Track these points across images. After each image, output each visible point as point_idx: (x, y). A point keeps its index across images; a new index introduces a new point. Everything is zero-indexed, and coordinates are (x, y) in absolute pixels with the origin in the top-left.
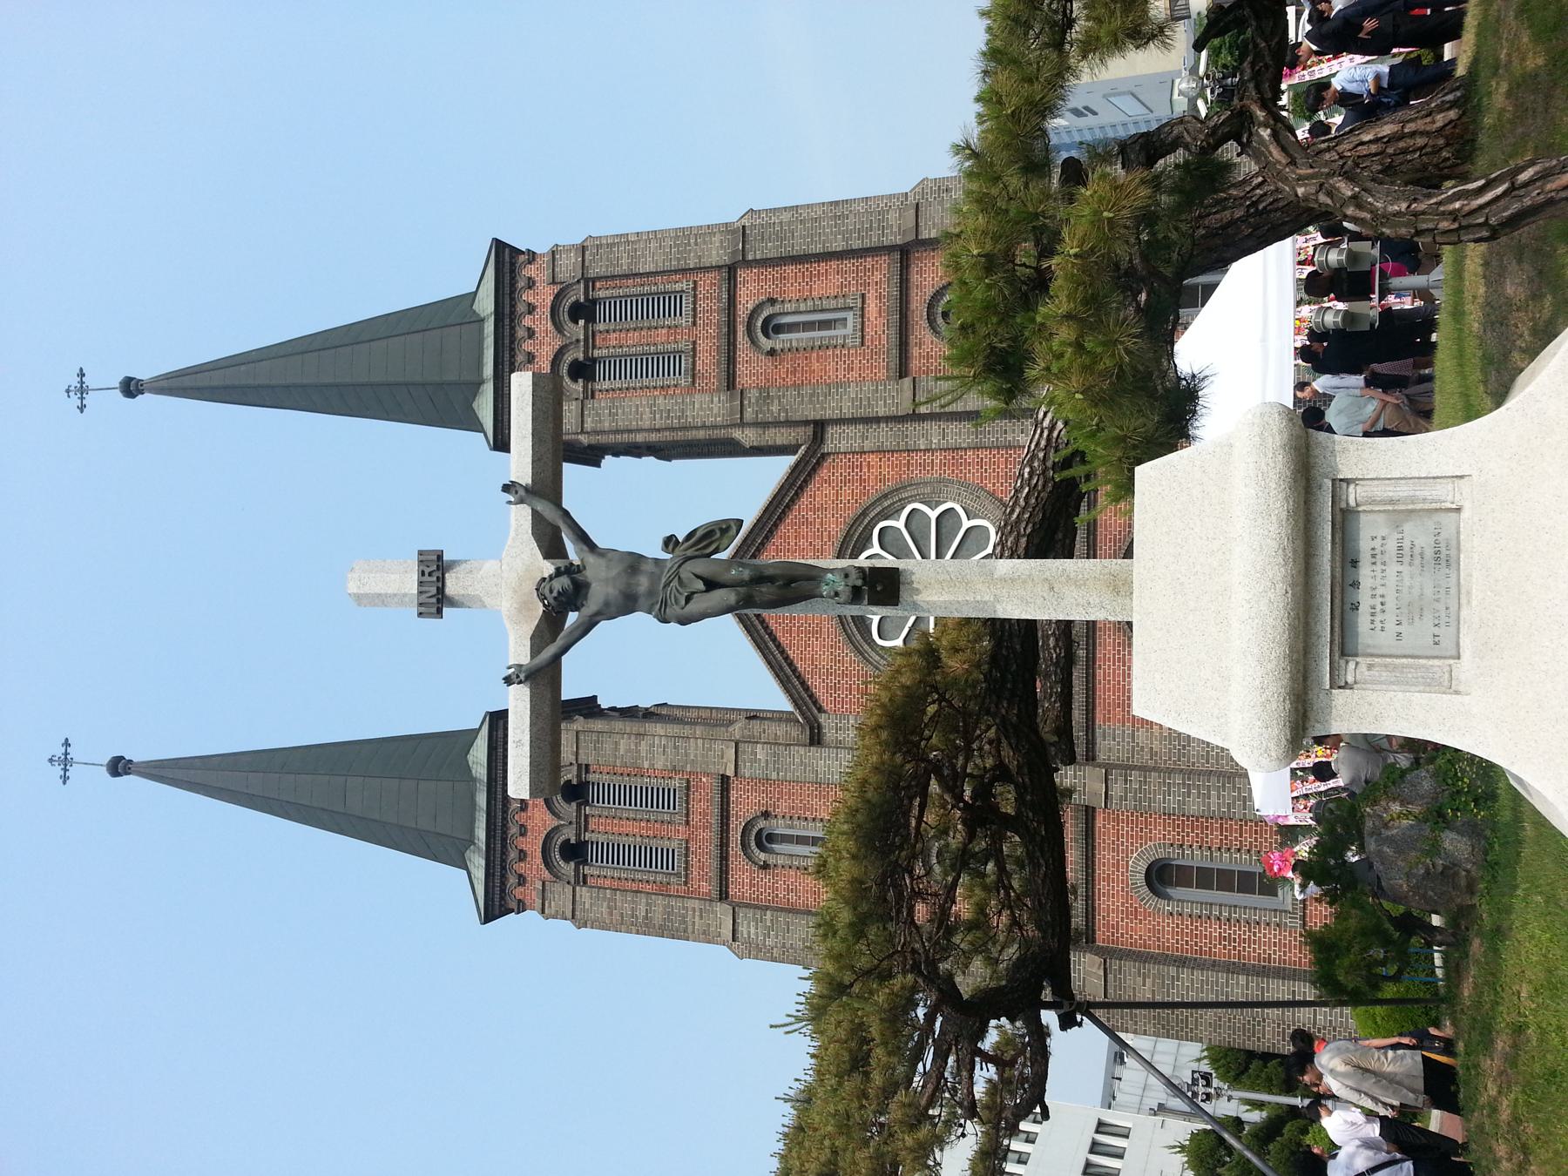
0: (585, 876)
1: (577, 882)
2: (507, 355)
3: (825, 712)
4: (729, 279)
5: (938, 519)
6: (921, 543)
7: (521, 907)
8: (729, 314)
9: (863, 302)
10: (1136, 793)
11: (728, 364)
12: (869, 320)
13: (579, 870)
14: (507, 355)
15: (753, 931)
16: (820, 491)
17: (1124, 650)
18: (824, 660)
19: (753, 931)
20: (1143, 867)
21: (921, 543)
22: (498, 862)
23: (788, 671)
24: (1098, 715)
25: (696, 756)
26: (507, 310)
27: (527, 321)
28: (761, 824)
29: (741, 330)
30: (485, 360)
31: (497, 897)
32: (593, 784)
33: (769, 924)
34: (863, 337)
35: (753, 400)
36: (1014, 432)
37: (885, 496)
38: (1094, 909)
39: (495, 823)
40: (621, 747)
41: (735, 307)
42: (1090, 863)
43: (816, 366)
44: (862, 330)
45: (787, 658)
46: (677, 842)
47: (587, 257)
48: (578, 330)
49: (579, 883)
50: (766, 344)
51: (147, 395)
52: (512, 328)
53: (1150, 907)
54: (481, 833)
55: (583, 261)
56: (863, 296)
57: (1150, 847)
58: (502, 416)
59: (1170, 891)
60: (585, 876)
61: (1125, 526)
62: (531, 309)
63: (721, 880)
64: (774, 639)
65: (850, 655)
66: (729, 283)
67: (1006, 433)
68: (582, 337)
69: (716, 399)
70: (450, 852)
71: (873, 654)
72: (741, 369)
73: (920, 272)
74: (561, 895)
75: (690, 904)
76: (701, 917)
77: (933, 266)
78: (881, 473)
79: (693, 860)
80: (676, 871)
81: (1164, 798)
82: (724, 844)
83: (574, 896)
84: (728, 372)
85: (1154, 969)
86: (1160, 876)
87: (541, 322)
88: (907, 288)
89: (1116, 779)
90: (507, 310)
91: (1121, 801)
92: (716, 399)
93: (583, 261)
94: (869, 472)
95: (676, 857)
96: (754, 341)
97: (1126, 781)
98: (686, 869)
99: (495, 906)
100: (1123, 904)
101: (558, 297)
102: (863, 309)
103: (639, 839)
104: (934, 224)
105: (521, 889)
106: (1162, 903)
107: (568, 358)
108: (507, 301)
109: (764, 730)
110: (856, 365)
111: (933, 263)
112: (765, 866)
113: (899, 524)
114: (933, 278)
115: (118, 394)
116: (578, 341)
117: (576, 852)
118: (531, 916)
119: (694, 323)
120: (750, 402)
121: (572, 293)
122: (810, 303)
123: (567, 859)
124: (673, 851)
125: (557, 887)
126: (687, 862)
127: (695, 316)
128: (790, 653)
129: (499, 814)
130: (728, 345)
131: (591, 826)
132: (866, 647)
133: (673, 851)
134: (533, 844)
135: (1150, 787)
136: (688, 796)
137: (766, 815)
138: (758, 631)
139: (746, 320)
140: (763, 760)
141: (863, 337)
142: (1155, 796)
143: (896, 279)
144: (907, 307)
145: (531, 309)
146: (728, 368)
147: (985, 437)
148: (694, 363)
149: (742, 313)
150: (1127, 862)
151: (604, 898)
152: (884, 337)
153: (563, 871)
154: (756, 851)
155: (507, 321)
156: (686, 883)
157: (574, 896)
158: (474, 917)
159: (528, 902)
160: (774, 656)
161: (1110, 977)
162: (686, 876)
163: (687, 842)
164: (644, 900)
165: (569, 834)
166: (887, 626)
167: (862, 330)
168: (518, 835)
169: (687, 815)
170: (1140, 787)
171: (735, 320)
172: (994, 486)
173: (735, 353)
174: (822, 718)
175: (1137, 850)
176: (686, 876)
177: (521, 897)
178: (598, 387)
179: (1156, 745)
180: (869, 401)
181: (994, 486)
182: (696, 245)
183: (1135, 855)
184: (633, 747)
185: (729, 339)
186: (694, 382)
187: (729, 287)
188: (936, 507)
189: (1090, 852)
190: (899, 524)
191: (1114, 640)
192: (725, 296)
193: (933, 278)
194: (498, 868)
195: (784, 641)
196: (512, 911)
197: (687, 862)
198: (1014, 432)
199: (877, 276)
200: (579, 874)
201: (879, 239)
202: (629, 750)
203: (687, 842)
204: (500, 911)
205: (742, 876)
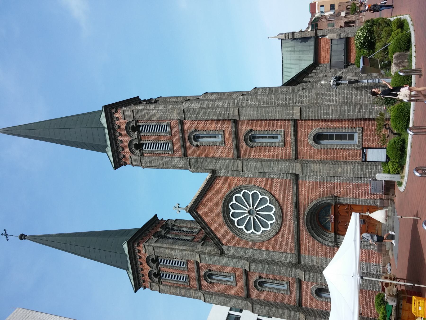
0: (143, 153)
3: (224, 245)
4: (181, 123)
5: (252, 195)
7: (125, 164)
8: (182, 134)
9: (224, 133)
11: (184, 149)
12: (226, 139)
13: (141, 152)
15: (209, 300)
16: (216, 186)
17: (308, 236)
18: (222, 232)
19: (209, 300)
20: (314, 290)
21: (247, 200)
22: (136, 277)
25: (188, 255)
27: (122, 153)
30: (107, 141)
32: (160, 259)
33: (214, 299)
34: (225, 143)
35: (193, 162)
37: (236, 189)
39: (134, 268)
40: (167, 252)
43: (211, 151)
44: (225, 142)
46: (186, 275)
48: (135, 135)
49: (141, 156)
50: (195, 143)
52: (118, 156)
53: (316, 299)
54: (109, 144)
55: (133, 115)
57: (313, 131)
60: (161, 282)
61: (307, 203)
62: (123, 149)
65: (229, 231)
66: (181, 124)
68: (137, 137)
69: (181, 160)
70: (102, 149)
71: (236, 230)
72: (188, 150)
73: (241, 125)
74: (136, 159)
75: (192, 291)
76: (195, 295)
77: (245, 123)
78: (234, 184)
79: (191, 280)
80: (168, 132)
81: (320, 280)
82: (199, 280)
85: (318, 319)
87: (145, 266)
89: (307, 274)
90: (111, 128)
91: (308, 280)
92: (181, 160)
93: (133, 115)
95: (170, 147)
96: (191, 143)
97: (310, 275)
98: (189, 282)
100: (309, 298)
102: (224, 135)
103: (175, 274)
105: (144, 283)
106: (319, 298)
107: (134, 143)
108: (111, 124)
109: (207, 249)
110: (224, 151)
111: (245, 123)
112: (211, 283)
113: (241, 195)
116: (136, 138)
117: (139, 146)
118: (129, 166)
120: (192, 163)
121: (131, 123)
122: (207, 132)
123: (137, 149)
124: (185, 277)
125: (154, 284)
126: (189, 280)
127: (171, 133)
128: (212, 229)
129: (135, 266)
131: (161, 270)
132: (234, 229)
133: (185, 277)
134: (144, 261)
135: (316, 277)
136: (187, 264)
138: (202, 224)
139: (189, 134)
141: (225, 143)
144: (238, 135)
145: (119, 127)
148: (173, 147)
149: (202, 273)
150: (310, 288)
151: (168, 288)
152: (231, 144)
153: (155, 280)
154: (208, 279)
155: (112, 131)
156: (190, 285)
158: (113, 169)
159: (146, 286)
162: (190, 283)
164: (179, 290)
166: (240, 222)
167: (225, 142)
169: (188, 269)
171: (184, 135)
174: (223, 247)
175: (313, 285)
176: (190, 283)
177: (144, 285)
178: (144, 152)
179: (317, 261)
180: (229, 166)
183: (312, 287)
184: (170, 252)
186: (174, 153)
187: (181, 126)
188: (251, 191)
189: (300, 285)
191: (305, 233)
194: (137, 279)
196: (123, 165)
197: (189, 280)
199: (227, 125)
201: (227, 117)
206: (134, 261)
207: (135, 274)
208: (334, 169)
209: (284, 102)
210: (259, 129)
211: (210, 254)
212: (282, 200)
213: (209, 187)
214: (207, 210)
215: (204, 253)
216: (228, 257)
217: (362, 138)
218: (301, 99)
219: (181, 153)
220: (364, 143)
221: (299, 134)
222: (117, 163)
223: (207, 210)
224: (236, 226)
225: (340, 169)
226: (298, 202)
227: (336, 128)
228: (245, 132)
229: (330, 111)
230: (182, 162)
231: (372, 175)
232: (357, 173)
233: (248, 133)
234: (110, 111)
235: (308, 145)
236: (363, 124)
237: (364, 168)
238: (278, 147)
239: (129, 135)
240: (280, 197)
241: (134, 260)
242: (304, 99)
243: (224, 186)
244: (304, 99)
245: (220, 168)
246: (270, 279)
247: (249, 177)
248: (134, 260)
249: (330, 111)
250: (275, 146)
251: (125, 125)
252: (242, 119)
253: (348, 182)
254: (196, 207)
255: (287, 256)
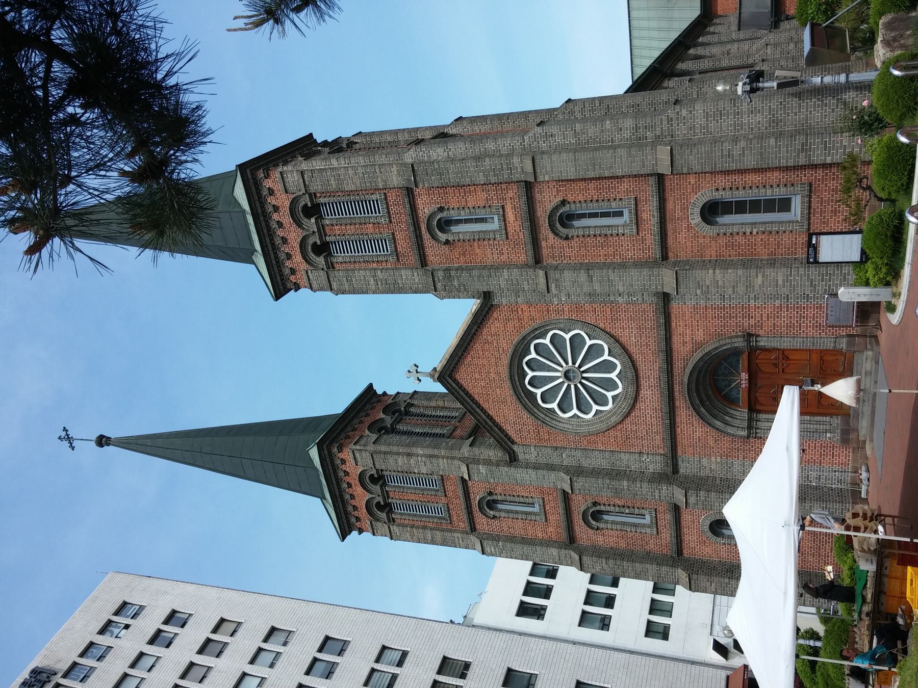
1: (328, 268)
2: (268, 240)
3: (516, 443)
6: (561, 351)
7: (297, 287)
8: (413, 217)
9: (504, 211)
10: (703, 502)
11: (419, 250)
14: (268, 240)
15: (493, 550)
16: (494, 326)
19: (493, 550)
20: (708, 523)
23: (491, 424)
24: (679, 451)
25: (444, 467)
26: (260, 211)
27: (288, 264)
28: (489, 498)
29: (426, 235)
31: (279, 279)
33: (501, 547)
35: (441, 278)
36: (615, 296)
38: (681, 540)
41: (416, 212)
42: (678, 528)
43: (478, 251)
45: (488, 416)
47: (306, 178)
50: (443, 237)
51: (111, 447)
55: (304, 182)
56: (503, 207)
58: (276, 279)
59: (718, 219)
60: (393, 519)
62: (289, 256)
63: (470, 523)
64: (479, 406)
65: (525, 415)
66: (409, 197)
67: (609, 296)
68: (316, 230)
69: (415, 274)
71: (540, 414)
72: (429, 252)
73: (541, 192)
74: (382, 527)
75: (456, 535)
79: (453, 513)
83: (390, 530)
84: (420, 254)
86: (711, 211)
88: (532, 203)
90: (260, 211)
91: (695, 505)
92: (415, 274)
93: (304, 182)
94: (523, 314)
95: (388, 244)
96: (434, 237)
99: (280, 288)
101: (294, 202)
102: (504, 215)
103: (419, 503)
104: (546, 171)
106: (719, 539)
108: (257, 203)
110: (505, 251)
112: (494, 517)
114: (549, 196)
115: (93, 443)
116: (314, 232)
117: (323, 249)
119: (390, 222)
122: (467, 211)
124: (441, 508)
126: (449, 514)
127: (390, 217)
130: (417, 238)
131: (391, 495)
132: (535, 410)
133: (441, 508)
137: (441, 209)
140: (484, 473)
142: (714, 503)
143: (524, 199)
144: (534, 215)
145: (276, 209)
146: (419, 252)
147: (596, 298)
149: (475, 499)
150: (699, 520)
152: (521, 234)
154: (488, 510)
155: (262, 218)
157: (390, 530)
159: (364, 527)
160: (481, 417)
161: (693, 582)
162: (450, 520)
163: (447, 504)
165: (316, 239)
166: (547, 396)
167: (506, 229)
168: (286, 259)
170: (706, 499)
171: (418, 221)
172: (604, 324)
173: (422, 241)
174: (515, 448)
176: (450, 520)
177: (295, 281)
178: (334, 260)
181: (604, 324)
182: (381, 173)
183: (703, 517)
184: (406, 461)
185: (416, 234)
186: (398, 259)
187: (410, 200)
190: (547, 341)
191: (686, 413)
192: (408, 206)
193: (549, 196)
194: (343, 515)
195: (486, 406)
197: (449, 514)
198: (615, 296)
200: (383, 491)
202: (404, 464)
203: (447, 504)
204: (284, 290)
205: (481, 521)
206: (334, 482)
207: (339, 506)
208: (747, 279)
209: (634, 135)
210: (581, 198)
211: (488, 462)
212: (636, 347)
213: (479, 327)
214: (477, 376)
215: (477, 462)
216: (527, 466)
217: (810, 207)
218: (672, 126)
219: (412, 258)
220: (814, 216)
221: (670, 205)
222: (278, 286)
223: (477, 376)
224: (539, 405)
225: (760, 277)
226: (669, 350)
227: (751, 188)
228: (549, 208)
229: (736, 152)
230: (416, 277)
231: (829, 287)
232: (798, 284)
233: (556, 208)
234: (253, 175)
235: (689, 227)
236: (812, 176)
237: (812, 272)
238: (623, 235)
239: (299, 224)
240: (630, 338)
241: (333, 479)
242: (678, 125)
243: (510, 324)
244: (678, 125)
245: (500, 286)
246: (614, 506)
247: (563, 302)
248: (333, 479)
249: (736, 152)
250: (618, 235)
251: (287, 204)
252: (540, 178)
253: (777, 303)
254: (453, 371)
255: (648, 460)
